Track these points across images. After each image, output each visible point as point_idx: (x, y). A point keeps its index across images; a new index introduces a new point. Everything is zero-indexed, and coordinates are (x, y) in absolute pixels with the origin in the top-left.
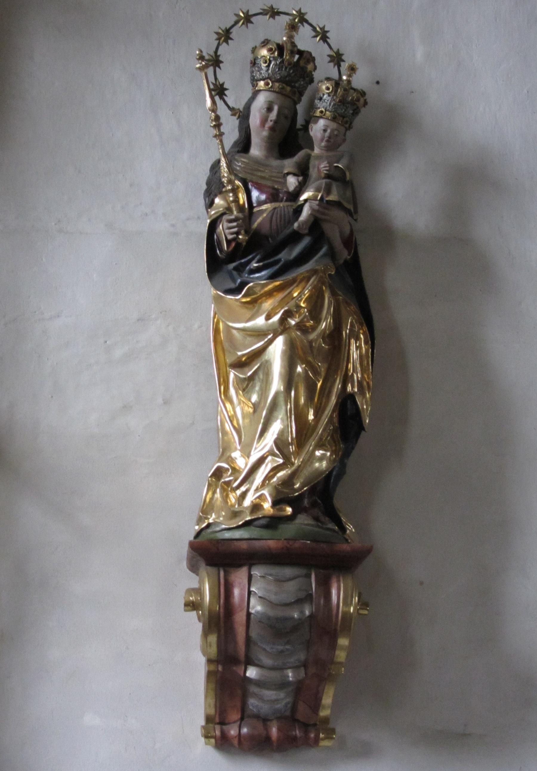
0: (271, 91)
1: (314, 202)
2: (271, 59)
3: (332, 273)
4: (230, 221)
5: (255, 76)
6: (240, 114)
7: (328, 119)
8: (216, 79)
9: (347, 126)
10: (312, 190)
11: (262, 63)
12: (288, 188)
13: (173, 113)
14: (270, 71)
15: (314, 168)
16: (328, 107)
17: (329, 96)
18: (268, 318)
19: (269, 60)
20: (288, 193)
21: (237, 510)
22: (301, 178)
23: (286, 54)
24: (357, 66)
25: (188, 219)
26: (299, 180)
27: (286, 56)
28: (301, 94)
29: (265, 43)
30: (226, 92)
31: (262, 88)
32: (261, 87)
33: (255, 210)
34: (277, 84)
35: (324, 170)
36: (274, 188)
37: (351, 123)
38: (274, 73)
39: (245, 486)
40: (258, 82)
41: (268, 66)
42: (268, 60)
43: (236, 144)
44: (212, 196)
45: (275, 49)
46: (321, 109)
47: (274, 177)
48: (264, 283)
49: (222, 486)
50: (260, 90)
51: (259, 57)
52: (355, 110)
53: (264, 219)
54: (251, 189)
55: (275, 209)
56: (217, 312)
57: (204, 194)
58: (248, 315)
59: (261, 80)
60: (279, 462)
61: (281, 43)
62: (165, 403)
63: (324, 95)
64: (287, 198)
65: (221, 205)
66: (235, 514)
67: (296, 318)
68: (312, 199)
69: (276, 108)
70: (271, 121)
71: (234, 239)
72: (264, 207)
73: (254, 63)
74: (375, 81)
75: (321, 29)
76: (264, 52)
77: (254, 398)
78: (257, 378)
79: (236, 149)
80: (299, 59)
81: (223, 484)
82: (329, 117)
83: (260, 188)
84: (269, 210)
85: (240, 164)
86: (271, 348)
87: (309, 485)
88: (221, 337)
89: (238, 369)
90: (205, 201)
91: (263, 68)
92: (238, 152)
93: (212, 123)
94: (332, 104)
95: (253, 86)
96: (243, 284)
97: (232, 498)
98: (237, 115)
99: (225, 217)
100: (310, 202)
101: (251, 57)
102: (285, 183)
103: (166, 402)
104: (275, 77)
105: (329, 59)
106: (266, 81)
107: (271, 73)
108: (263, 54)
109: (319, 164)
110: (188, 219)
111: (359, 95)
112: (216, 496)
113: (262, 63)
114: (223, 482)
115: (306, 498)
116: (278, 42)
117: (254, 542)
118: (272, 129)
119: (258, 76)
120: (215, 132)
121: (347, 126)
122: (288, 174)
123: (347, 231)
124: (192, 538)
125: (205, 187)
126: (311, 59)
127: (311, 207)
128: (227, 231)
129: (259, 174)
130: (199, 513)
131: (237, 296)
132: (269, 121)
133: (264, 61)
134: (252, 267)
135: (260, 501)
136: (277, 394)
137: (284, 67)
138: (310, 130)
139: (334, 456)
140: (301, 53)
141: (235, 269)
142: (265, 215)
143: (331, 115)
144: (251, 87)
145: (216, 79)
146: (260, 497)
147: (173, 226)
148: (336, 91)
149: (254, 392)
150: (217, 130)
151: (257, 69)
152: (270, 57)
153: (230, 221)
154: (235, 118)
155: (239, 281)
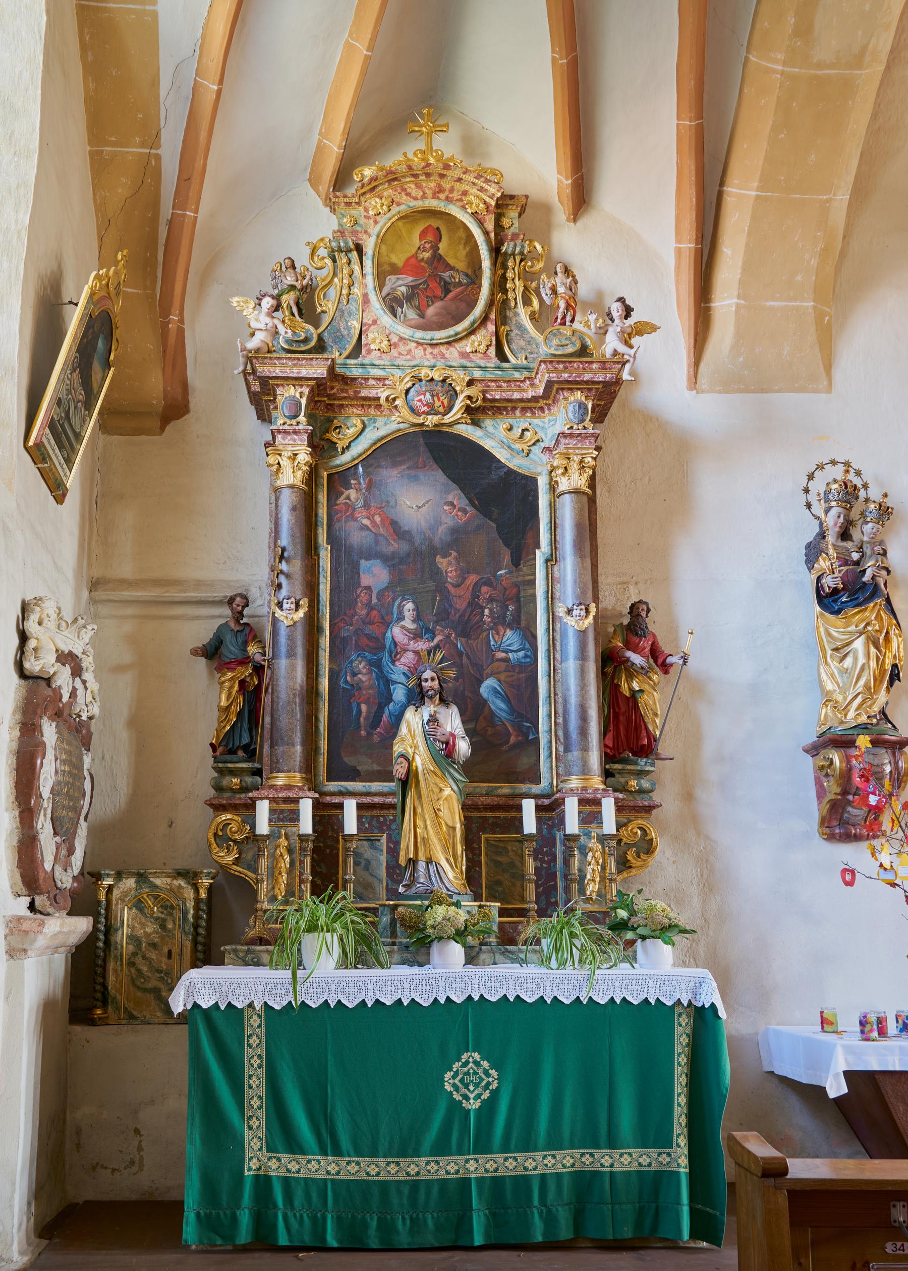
20: (853, 561)
69: (842, 516)
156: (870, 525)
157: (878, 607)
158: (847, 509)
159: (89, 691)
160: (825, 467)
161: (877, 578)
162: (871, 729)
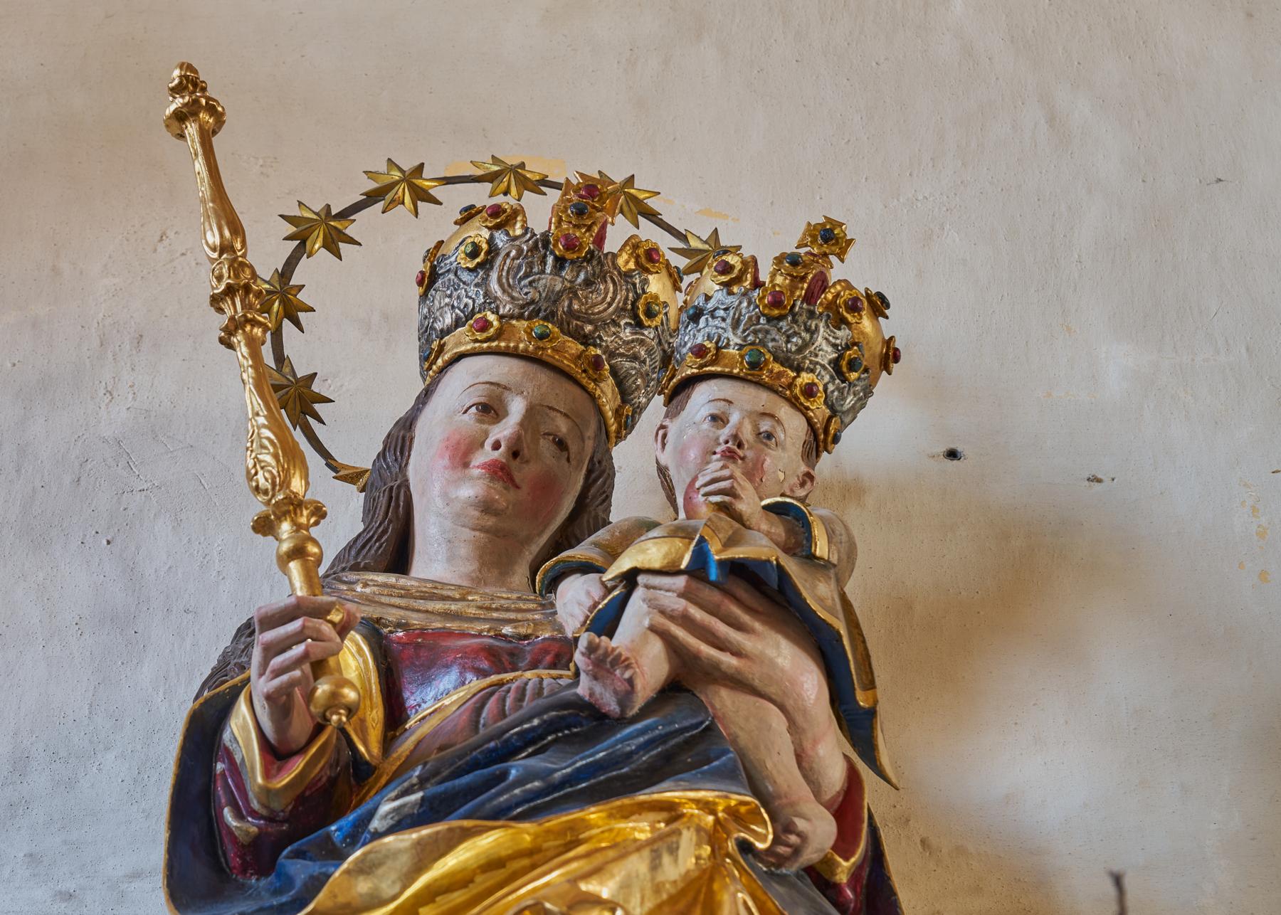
13: (109, 542)
38: (509, 285)
74: (943, 448)
100: (647, 587)
118: (500, 473)
137: (550, 260)
145: (280, 357)
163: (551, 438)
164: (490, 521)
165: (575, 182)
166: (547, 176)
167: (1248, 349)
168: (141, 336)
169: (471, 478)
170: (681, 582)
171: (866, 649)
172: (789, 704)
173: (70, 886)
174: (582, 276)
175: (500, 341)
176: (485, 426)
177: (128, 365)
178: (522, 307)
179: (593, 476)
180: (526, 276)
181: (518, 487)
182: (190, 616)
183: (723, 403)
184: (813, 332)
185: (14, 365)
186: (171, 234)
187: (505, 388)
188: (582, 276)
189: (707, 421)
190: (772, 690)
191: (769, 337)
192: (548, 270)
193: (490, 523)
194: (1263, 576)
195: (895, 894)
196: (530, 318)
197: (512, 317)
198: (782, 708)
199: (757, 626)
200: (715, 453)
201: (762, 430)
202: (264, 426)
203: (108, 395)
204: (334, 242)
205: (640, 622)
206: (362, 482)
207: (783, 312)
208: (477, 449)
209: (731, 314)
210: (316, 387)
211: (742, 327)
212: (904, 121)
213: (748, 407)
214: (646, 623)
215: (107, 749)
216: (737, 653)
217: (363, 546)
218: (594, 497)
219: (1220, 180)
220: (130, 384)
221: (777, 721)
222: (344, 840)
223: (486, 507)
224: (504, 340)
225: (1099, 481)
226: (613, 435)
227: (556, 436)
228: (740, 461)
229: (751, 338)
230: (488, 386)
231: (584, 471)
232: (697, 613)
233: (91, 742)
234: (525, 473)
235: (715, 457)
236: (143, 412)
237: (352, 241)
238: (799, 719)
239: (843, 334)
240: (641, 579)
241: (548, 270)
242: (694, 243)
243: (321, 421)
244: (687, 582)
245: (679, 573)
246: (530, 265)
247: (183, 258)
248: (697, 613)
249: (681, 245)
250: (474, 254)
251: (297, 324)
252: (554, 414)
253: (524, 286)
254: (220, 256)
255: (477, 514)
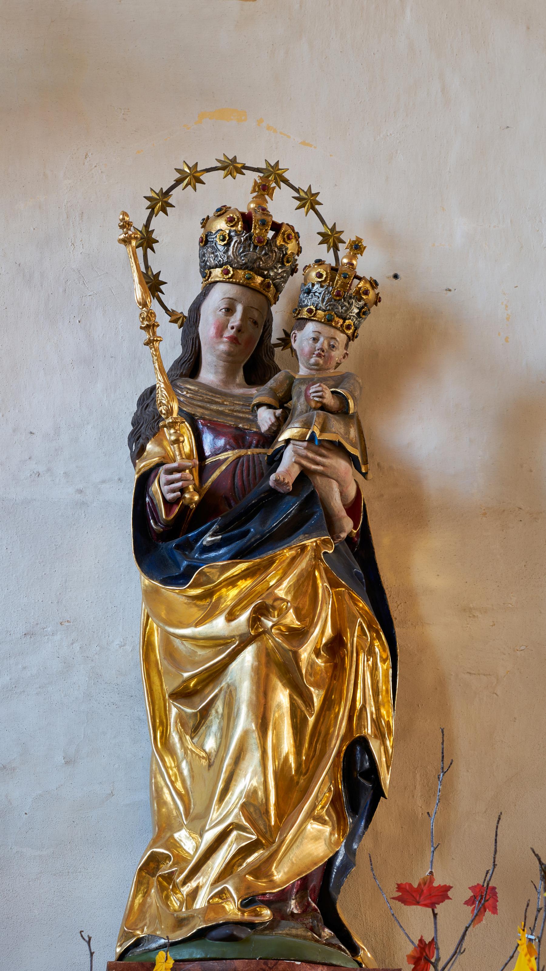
0: (232, 283)
1: (300, 443)
2: (232, 234)
3: (329, 552)
4: (170, 472)
5: (207, 261)
6: (183, 319)
7: (320, 322)
8: (147, 267)
9: (350, 332)
10: (297, 425)
11: (218, 241)
12: (258, 427)
13: (79, 322)
14: (230, 253)
15: (298, 398)
16: (321, 302)
17: (322, 286)
18: (231, 617)
19: (229, 234)
20: (259, 434)
21: (184, 915)
22: (279, 412)
23: (255, 226)
24: (364, 244)
25: (104, 482)
26: (276, 414)
27: (256, 231)
28: (278, 289)
29: (221, 212)
30: (162, 287)
31: (218, 279)
32: (217, 276)
33: (208, 461)
34: (241, 273)
35: (314, 397)
36: (237, 428)
37: (356, 329)
38: (236, 255)
39: (195, 881)
40: (212, 270)
41: (228, 245)
42: (227, 236)
43: (178, 363)
44: (141, 441)
45: (238, 219)
46: (309, 307)
47: (236, 411)
48: (223, 565)
49: (160, 883)
50: (216, 282)
51: (214, 232)
52: (363, 308)
53: (222, 473)
54: (203, 431)
55: (239, 458)
56: (150, 614)
57: (129, 439)
58: (198, 614)
59: (216, 267)
60: (251, 838)
61: (246, 211)
62: (67, 763)
63: (313, 285)
64: (258, 442)
65: (155, 453)
66: (180, 922)
67: (274, 617)
68: (297, 438)
69: (239, 308)
70: (232, 328)
71: (177, 501)
72: (222, 457)
73: (205, 241)
74: (392, 274)
75: (306, 193)
76: (221, 225)
77: (211, 744)
78: (213, 712)
79: (179, 372)
80: (275, 237)
81: (160, 879)
82: (321, 319)
83: (217, 432)
84: (230, 460)
85: (185, 393)
86: (234, 666)
87: (299, 875)
88: (155, 656)
89: (183, 700)
90: (131, 449)
91: (219, 247)
92: (182, 375)
93: (144, 324)
94: (327, 298)
95: (204, 277)
96: (192, 569)
97: (175, 902)
98: (180, 322)
99: (162, 469)
100: (294, 444)
101: (200, 232)
102: (254, 421)
103: (69, 762)
104: (238, 262)
105: (320, 238)
106: (225, 267)
107: (232, 255)
108: (220, 226)
109: (308, 389)
110: (104, 482)
111: (368, 286)
112: (149, 900)
113: (218, 241)
114: (160, 875)
115: (293, 900)
116: (241, 210)
117: (211, 963)
118: (234, 340)
119: (213, 261)
120: (145, 336)
121: (350, 332)
122: (259, 405)
123: (352, 493)
124: (113, 959)
125: (130, 428)
126: (293, 235)
127: (295, 452)
128: (165, 488)
129: (214, 407)
130: (122, 928)
131: (183, 587)
132: (229, 328)
133: (222, 237)
134: (204, 543)
135: (220, 901)
136: (246, 734)
137: (252, 246)
138: (292, 340)
139: (336, 836)
140: (276, 227)
141: (178, 547)
142: (223, 467)
143: (325, 315)
144: (201, 279)
145: (147, 267)
146: (220, 894)
147: (80, 491)
148: (333, 279)
149: (210, 735)
150: (151, 334)
151: (210, 250)
152: (230, 232)
153: (170, 472)
154: (176, 326)
155: (185, 563)
156: (310, 328)
157: (303, 564)
158: (254, 290)
159: (143, 464)
160: (204, 177)
161: (319, 481)
162: (247, 941)
163: (252, 320)
164: (230, 359)
165: (258, 182)
166: (245, 164)
167: (511, 221)
168: (82, 213)
169: (223, 342)
170: (305, 444)
171: (365, 444)
172: (339, 479)
173: (81, 486)
174: (264, 252)
175: (233, 279)
176: (228, 318)
177: (79, 229)
178: (241, 265)
179: (266, 328)
180: (243, 252)
181: (240, 344)
182: (113, 359)
183: (317, 333)
184: (351, 305)
185: (34, 229)
186: (90, 154)
187: (235, 300)
188: (264, 252)
189: (311, 340)
190: (334, 476)
191: (335, 307)
192: (251, 250)
193: (230, 359)
194: (507, 340)
195: (370, 534)
196: (244, 269)
197: (238, 268)
198: (337, 481)
199: (330, 455)
200: (314, 354)
201: (331, 344)
202: (163, 388)
203: (73, 246)
204: (165, 207)
205: (291, 459)
206: (180, 322)
207: (340, 298)
208: (226, 329)
209: (322, 295)
210: (161, 278)
211: (325, 303)
212: (384, 90)
213: (326, 335)
214: (293, 460)
215: (88, 423)
216: (323, 465)
217: (183, 363)
218: (266, 336)
219: (508, 127)
220: (81, 240)
221: (335, 485)
222: (193, 541)
223: (229, 354)
224: (235, 279)
225: (450, 290)
226: (272, 300)
227: (253, 320)
228: (323, 358)
229: (328, 308)
230: (229, 299)
231: (262, 328)
232: (311, 455)
233: (82, 420)
234: (243, 338)
235: (314, 355)
236: (87, 255)
237: (172, 206)
238: (342, 483)
239: (362, 303)
240: (291, 441)
241: (251, 250)
242: (302, 194)
243: (163, 293)
244: (307, 444)
245: (305, 441)
246: (245, 247)
247: (96, 168)
248: (311, 455)
249: (297, 195)
250: (223, 240)
251: (153, 250)
252: (253, 309)
253: (242, 256)
254: (143, 308)
255: (225, 356)
